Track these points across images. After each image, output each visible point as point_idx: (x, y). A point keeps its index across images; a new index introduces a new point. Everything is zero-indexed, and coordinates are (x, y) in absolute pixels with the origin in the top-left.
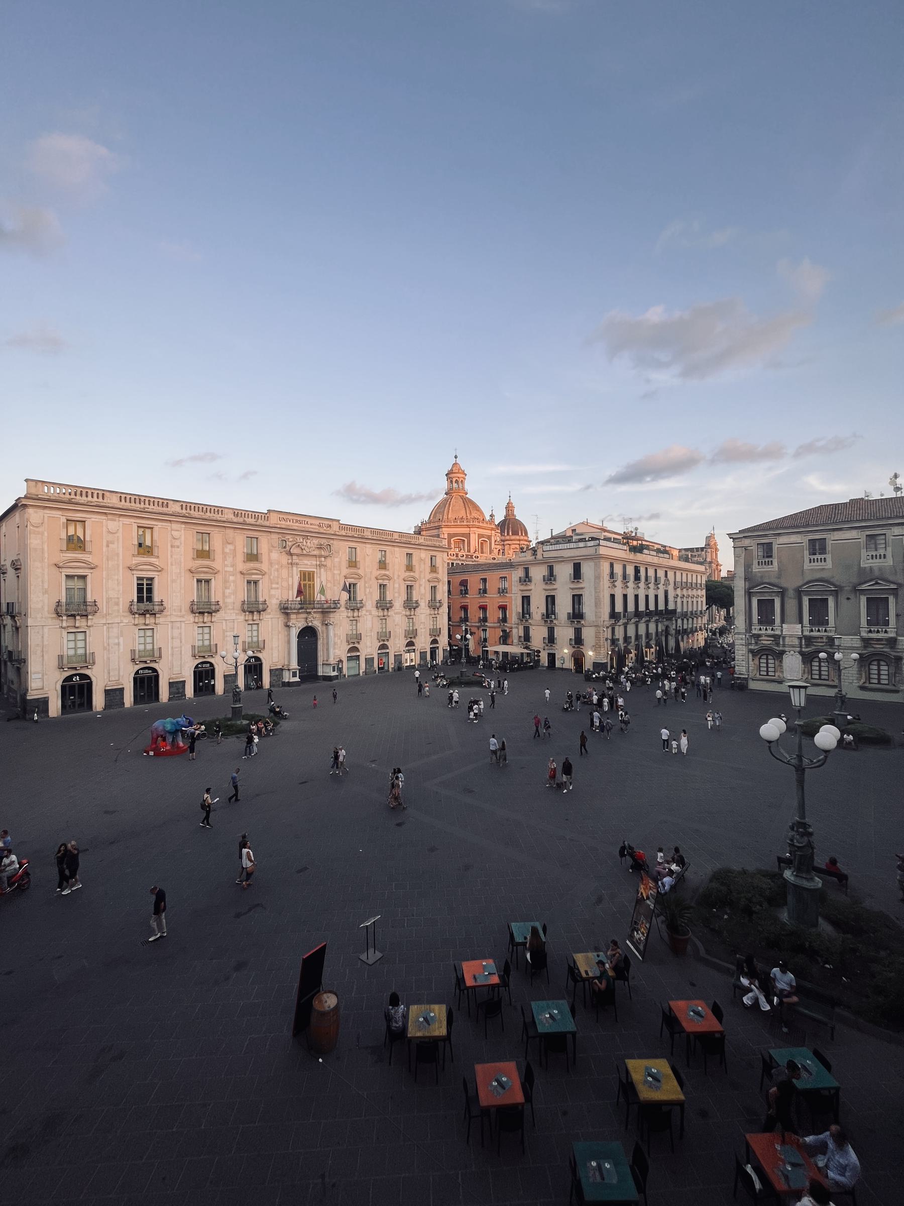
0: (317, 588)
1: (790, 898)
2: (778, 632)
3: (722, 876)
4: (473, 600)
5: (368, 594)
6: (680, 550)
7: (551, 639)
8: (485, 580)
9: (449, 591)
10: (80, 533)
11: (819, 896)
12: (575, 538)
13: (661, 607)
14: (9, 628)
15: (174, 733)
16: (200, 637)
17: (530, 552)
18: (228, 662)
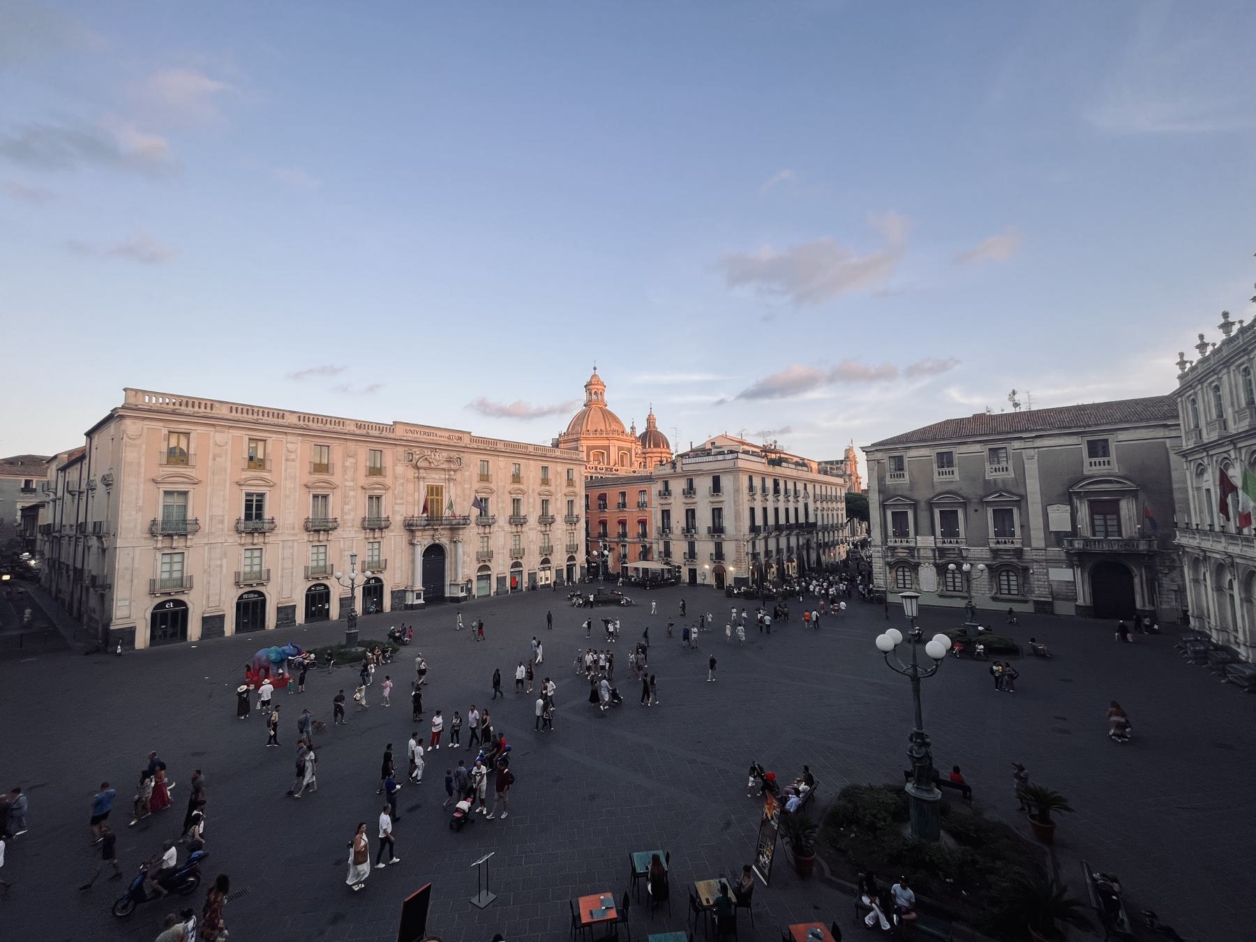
0: (445, 504)
1: (912, 811)
2: (912, 544)
3: (849, 794)
4: (612, 515)
5: (500, 508)
6: (819, 463)
7: (692, 554)
8: (623, 494)
9: (587, 506)
10: (183, 446)
11: (941, 809)
12: (714, 451)
13: (802, 520)
14: (94, 550)
15: (279, 663)
16: (315, 557)
17: (669, 466)
18: (345, 583)
